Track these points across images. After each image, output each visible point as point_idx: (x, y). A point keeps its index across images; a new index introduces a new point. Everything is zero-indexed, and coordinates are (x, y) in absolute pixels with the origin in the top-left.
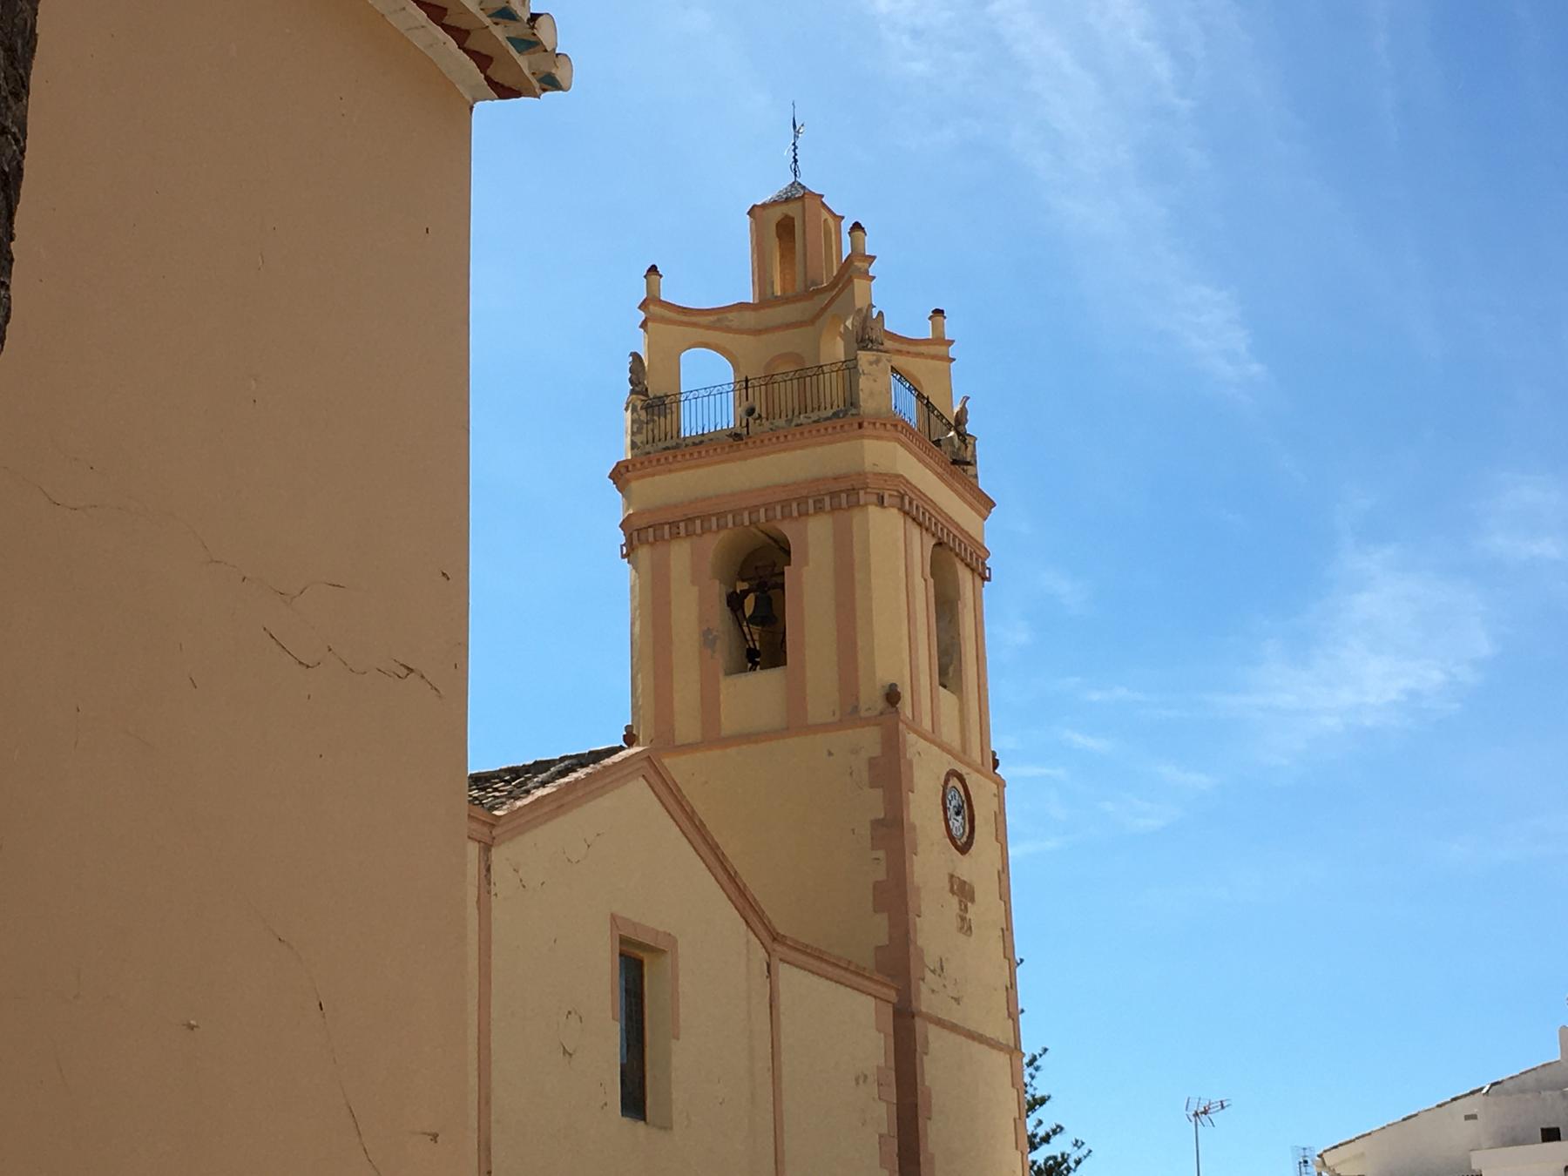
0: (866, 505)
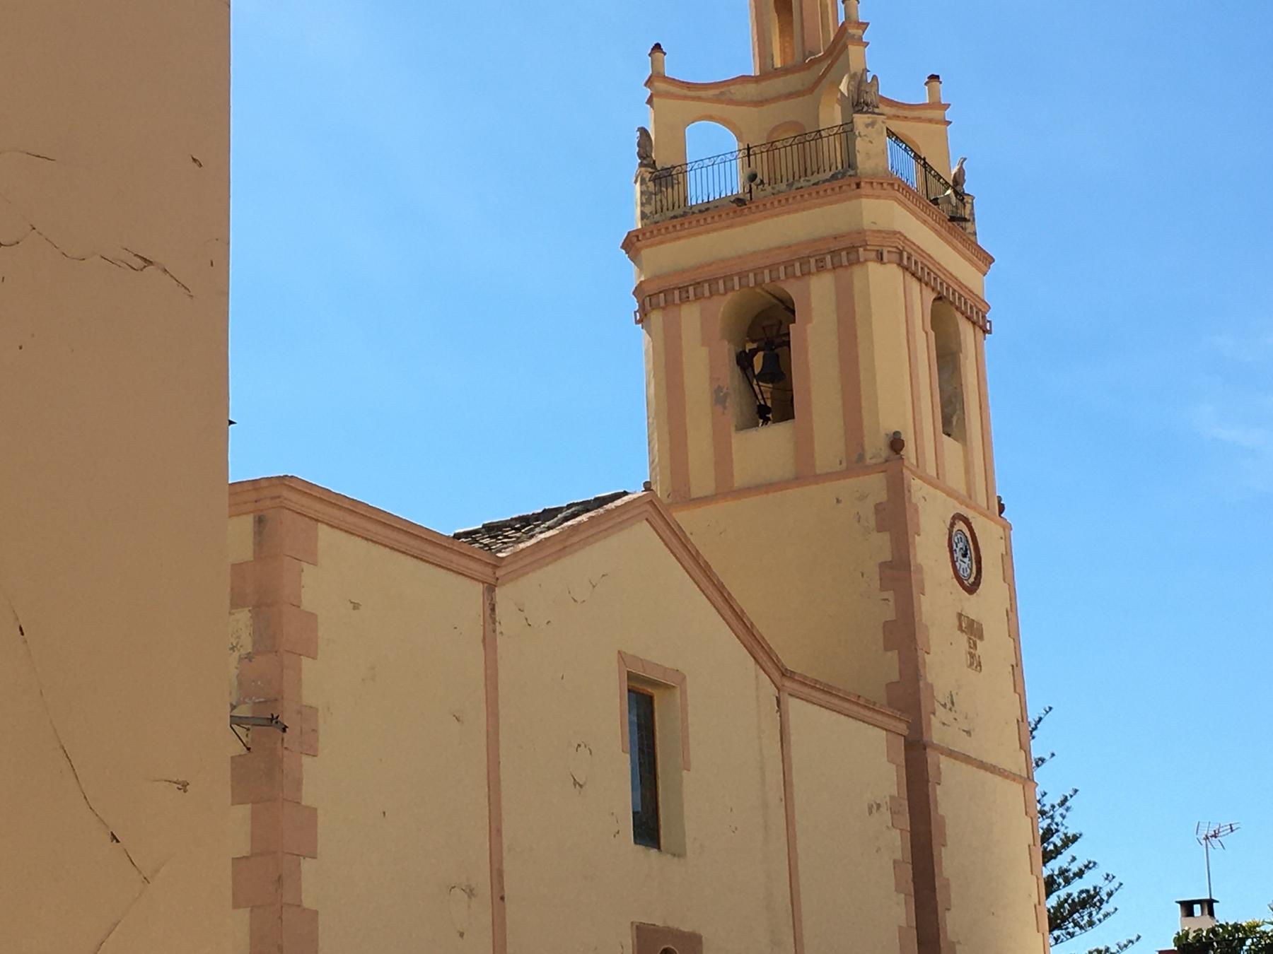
0: (866, 261)
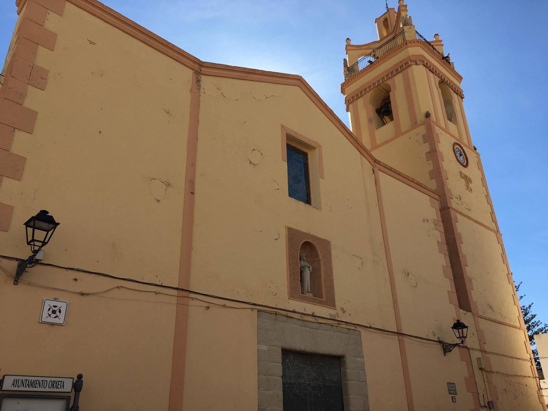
0: (411, 65)
